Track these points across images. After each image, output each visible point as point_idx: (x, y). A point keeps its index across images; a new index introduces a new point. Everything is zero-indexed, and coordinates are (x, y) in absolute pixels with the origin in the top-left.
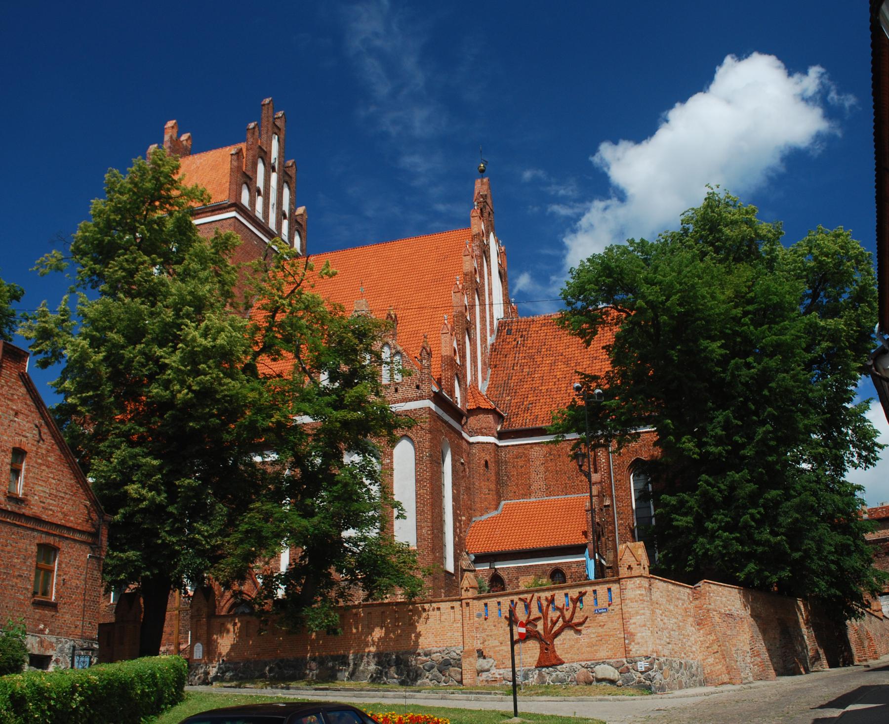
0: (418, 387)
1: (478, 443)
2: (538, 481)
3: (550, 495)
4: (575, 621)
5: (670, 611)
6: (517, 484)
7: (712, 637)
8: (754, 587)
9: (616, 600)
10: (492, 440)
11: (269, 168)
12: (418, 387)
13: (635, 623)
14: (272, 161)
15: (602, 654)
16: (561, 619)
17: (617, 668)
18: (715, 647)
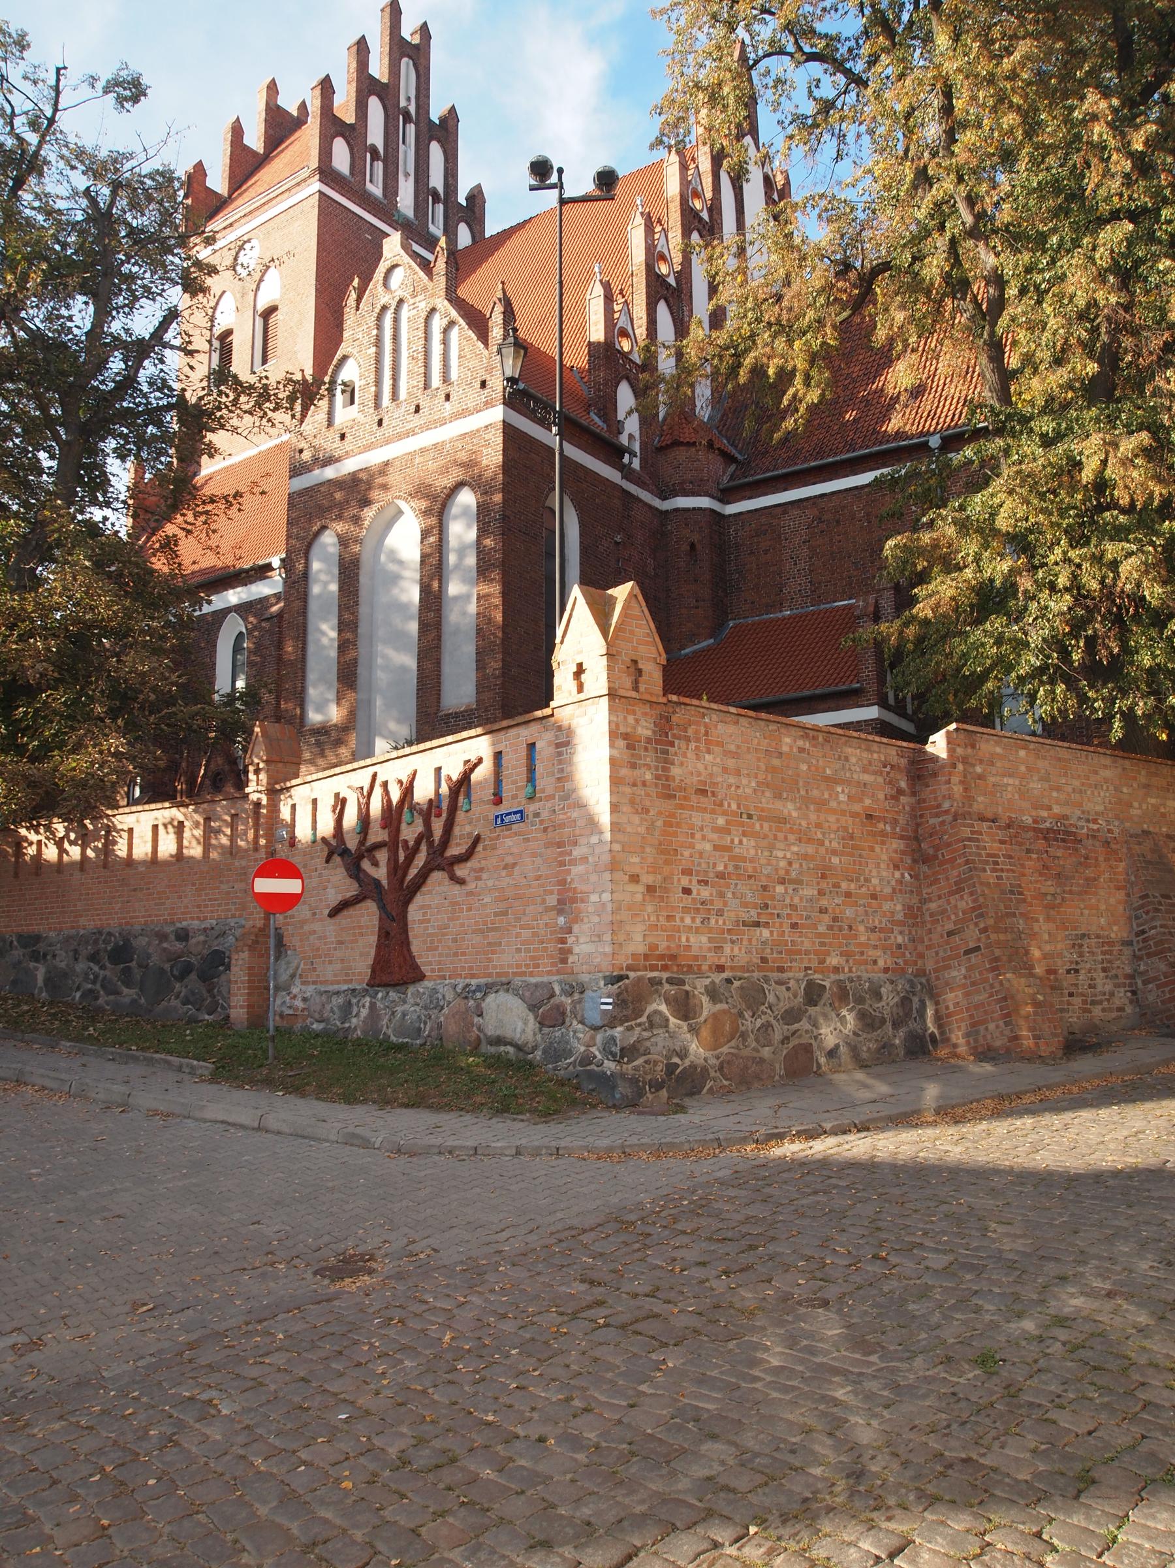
0: (483, 384)
3: (820, 602)
4: (454, 851)
5: (782, 820)
7: (964, 903)
8: (1106, 744)
9: (544, 782)
10: (704, 502)
12: (483, 384)
13: (584, 859)
14: (403, 103)
15: (508, 959)
16: (424, 847)
17: (533, 1008)
18: (972, 935)
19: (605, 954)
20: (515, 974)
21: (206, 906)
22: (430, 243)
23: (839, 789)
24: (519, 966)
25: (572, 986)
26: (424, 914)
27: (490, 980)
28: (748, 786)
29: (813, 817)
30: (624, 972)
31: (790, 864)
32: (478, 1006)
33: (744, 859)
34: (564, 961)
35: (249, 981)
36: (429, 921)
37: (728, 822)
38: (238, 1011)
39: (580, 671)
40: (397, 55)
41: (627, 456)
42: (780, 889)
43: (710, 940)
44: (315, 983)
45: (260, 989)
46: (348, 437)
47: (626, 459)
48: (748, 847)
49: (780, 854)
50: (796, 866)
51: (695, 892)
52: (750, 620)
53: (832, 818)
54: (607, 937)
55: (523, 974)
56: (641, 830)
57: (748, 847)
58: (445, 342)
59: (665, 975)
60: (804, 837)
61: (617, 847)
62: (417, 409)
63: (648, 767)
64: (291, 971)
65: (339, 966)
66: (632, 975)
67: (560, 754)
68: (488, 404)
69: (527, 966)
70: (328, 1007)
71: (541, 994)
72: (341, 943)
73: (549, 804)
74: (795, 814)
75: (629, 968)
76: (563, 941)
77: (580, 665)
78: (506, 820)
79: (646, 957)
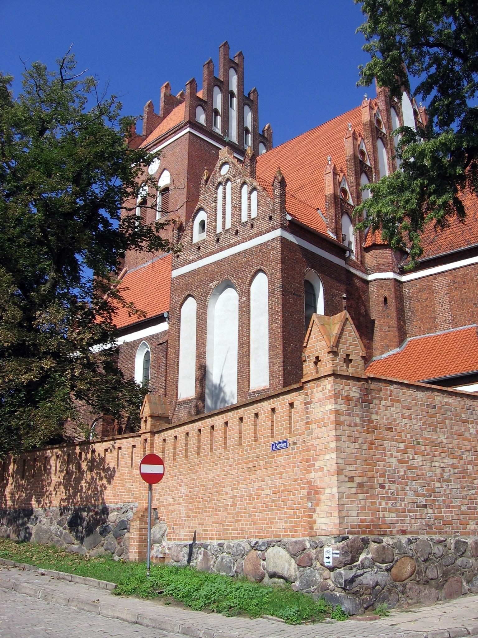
0: (270, 218)
1: (375, 280)
2: (443, 313)
3: (457, 326)
5: (437, 445)
6: (421, 319)
11: (228, 95)
12: (270, 218)
13: (322, 469)
15: (280, 526)
17: (293, 555)
19: (335, 525)
20: (284, 536)
21: (118, 496)
22: (242, 152)
23: (470, 426)
24: (286, 531)
25: (316, 543)
26: (234, 501)
27: (270, 540)
28: (417, 425)
29: (455, 442)
30: (346, 535)
31: (443, 470)
32: (263, 555)
33: (416, 468)
34: (311, 528)
35: (140, 538)
36: (236, 505)
37: (406, 446)
38: (133, 555)
39: (317, 360)
40: (227, 67)
41: (348, 252)
42: (438, 485)
43: (398, 516)
44: (174, 539)
45: (146, 543)
46: (202, 249)
47: (347, 254)
48: (418, 461)
49: (437, 464)
50: (447, 470)
51: (387, 488)
52: (419, 337)
53: (467, 443)
54: (336, 514)
55: (288, 536)
56: (354, 451)
57: (418, 461)
58: (249, 198)
59: (371, 537)
60: (451, 454)
61: (340, 461)
62: (237, 232)
63: (358, 416)
64: (162, 532)
65: (187, 530)
66: (350, 537)
67: (307, 408)
68: (273, 228)
69: (291, 531)
70: (181, 553)
71: (298, 547)
72: (188, 517)
73: (301, 437)
74: (445, 441)
75: (349, 533)
76: (310, 516)
77: (317, 358)
78: (278, 446)
79: (359, 526)
